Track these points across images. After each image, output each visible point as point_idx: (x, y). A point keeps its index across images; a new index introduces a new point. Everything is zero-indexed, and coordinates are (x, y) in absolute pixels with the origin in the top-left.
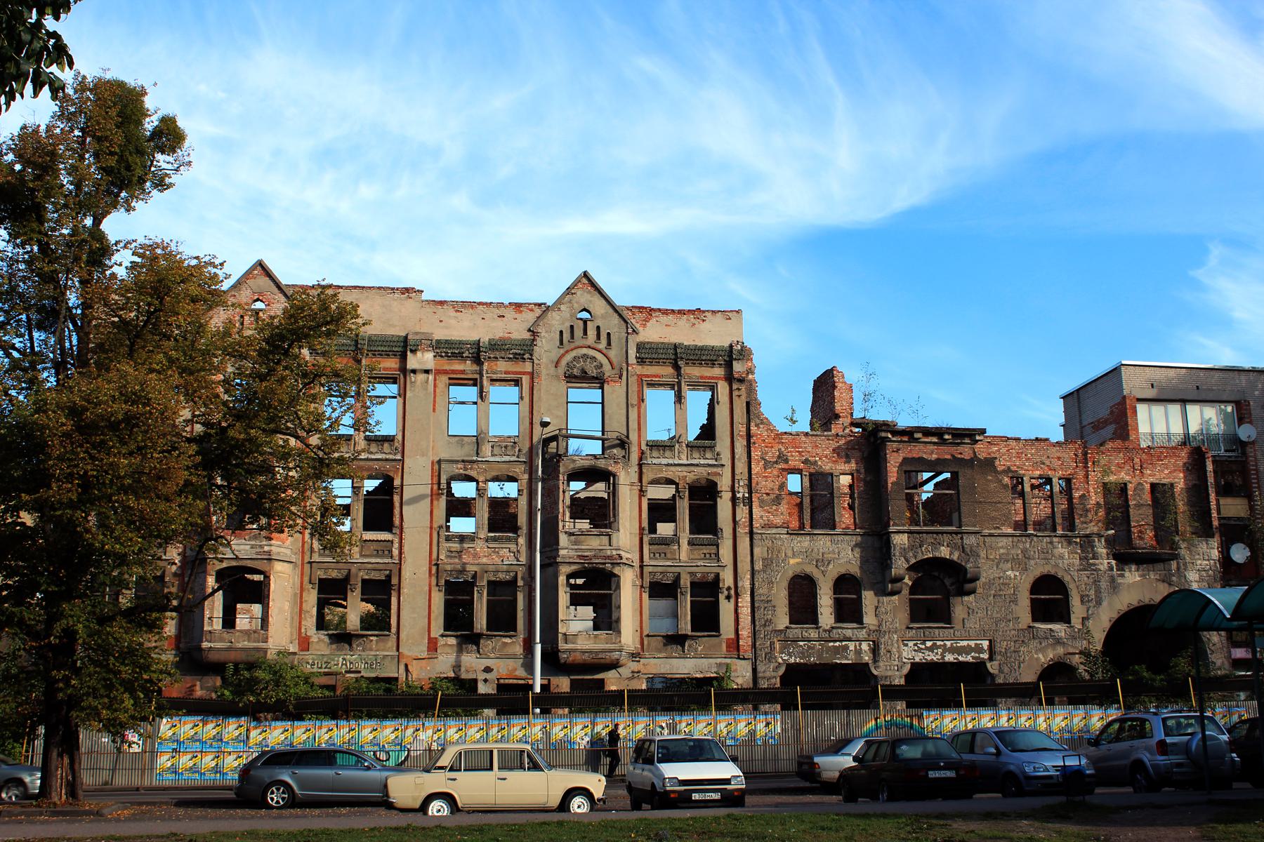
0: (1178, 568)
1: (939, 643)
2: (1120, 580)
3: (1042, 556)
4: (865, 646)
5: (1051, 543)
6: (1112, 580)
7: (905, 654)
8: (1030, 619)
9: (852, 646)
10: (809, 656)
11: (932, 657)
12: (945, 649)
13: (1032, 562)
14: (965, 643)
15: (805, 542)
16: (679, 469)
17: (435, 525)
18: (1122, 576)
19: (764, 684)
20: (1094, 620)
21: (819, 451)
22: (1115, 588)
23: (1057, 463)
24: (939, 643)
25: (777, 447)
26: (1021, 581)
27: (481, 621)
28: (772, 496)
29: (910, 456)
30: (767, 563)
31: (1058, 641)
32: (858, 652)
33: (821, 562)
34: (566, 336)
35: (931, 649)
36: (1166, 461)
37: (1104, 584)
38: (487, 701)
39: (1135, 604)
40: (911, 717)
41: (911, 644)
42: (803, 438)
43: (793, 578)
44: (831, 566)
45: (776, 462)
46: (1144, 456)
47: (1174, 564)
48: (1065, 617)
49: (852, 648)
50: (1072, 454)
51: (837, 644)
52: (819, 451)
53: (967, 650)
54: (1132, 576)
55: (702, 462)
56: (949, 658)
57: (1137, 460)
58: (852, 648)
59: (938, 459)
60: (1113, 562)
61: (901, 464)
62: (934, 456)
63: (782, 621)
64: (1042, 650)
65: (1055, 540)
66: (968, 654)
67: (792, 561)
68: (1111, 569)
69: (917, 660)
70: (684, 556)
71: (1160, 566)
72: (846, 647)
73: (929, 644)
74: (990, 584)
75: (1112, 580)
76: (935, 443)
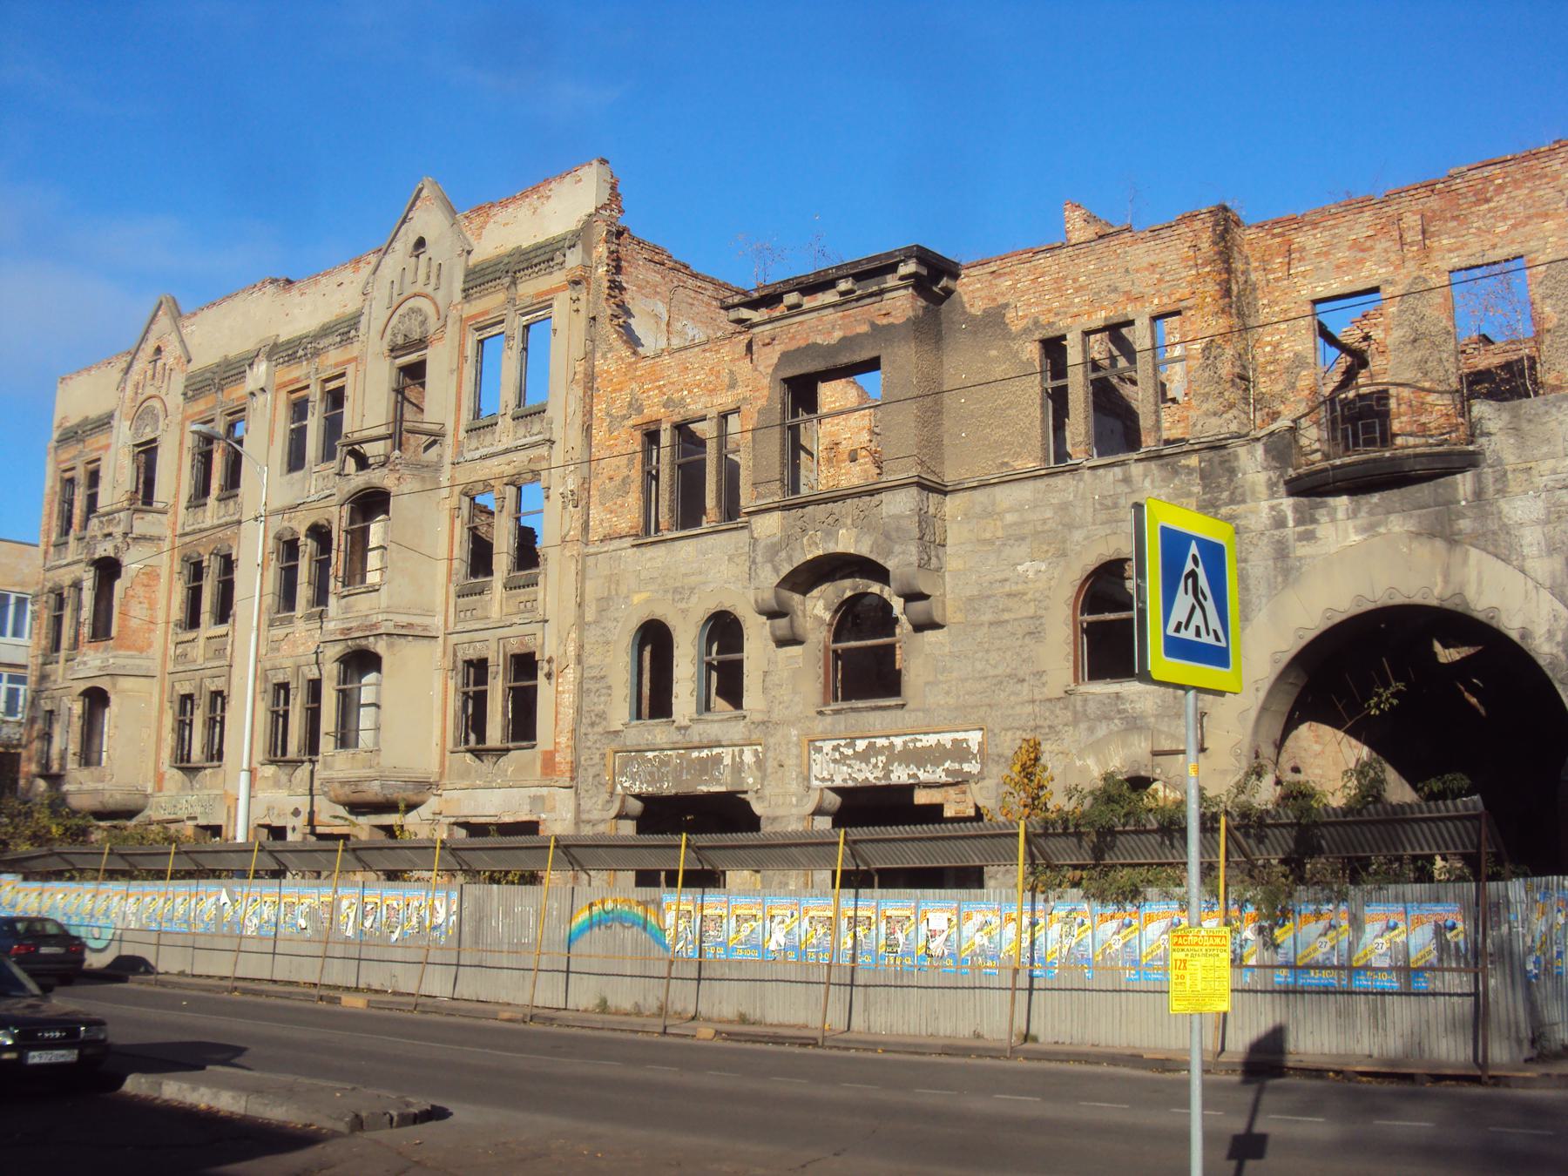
0: (1479, 494)
1: (881, 742)
2: (1302, 549)
3: (1103, 516)
4: (748, 757)
5: (1127, 480)
6: (1281, 552)
7: (816, 769)
8: (1068, 675)
9: (727, 756)
10: (661, 780)
13: (1078, 535)
14: (931, 740)
15: (656, 557)
16: (495, 461)
17: (590, 596)
18: (1309, 537)
22: (1286, 572)
24: (881, 742)
26: (1052, 591)
27: (495, 731)
28: (618, 480)
29: (793, 346)
30: (604, 603)
31: (1134, 724)
32: (738, 767)
35: (864, 757)
36: (1502, 199)
40: (645, 904)
41: (827, 746)
42: (666, 359)
43: (1453, 622)
44: (694, 599)
45: (624, 417)
47: (1464, 483)
49: (727, 760)
50: (1185, 249)
51: (704, 753)
55: (529, 440)
58: (727, 760)
59: (844, 339)
61: (777, 367)
62: (838, 335)
64: (1096, 747)
66: (937, 762)
67: (636, 599)
68: (1280, 523)
70: (495, 612)
71: (1424, 491)
72: (718, 760)
73: (861, 745)
74: (971, 604)
75: (1281, 552)
76: (834, 305)
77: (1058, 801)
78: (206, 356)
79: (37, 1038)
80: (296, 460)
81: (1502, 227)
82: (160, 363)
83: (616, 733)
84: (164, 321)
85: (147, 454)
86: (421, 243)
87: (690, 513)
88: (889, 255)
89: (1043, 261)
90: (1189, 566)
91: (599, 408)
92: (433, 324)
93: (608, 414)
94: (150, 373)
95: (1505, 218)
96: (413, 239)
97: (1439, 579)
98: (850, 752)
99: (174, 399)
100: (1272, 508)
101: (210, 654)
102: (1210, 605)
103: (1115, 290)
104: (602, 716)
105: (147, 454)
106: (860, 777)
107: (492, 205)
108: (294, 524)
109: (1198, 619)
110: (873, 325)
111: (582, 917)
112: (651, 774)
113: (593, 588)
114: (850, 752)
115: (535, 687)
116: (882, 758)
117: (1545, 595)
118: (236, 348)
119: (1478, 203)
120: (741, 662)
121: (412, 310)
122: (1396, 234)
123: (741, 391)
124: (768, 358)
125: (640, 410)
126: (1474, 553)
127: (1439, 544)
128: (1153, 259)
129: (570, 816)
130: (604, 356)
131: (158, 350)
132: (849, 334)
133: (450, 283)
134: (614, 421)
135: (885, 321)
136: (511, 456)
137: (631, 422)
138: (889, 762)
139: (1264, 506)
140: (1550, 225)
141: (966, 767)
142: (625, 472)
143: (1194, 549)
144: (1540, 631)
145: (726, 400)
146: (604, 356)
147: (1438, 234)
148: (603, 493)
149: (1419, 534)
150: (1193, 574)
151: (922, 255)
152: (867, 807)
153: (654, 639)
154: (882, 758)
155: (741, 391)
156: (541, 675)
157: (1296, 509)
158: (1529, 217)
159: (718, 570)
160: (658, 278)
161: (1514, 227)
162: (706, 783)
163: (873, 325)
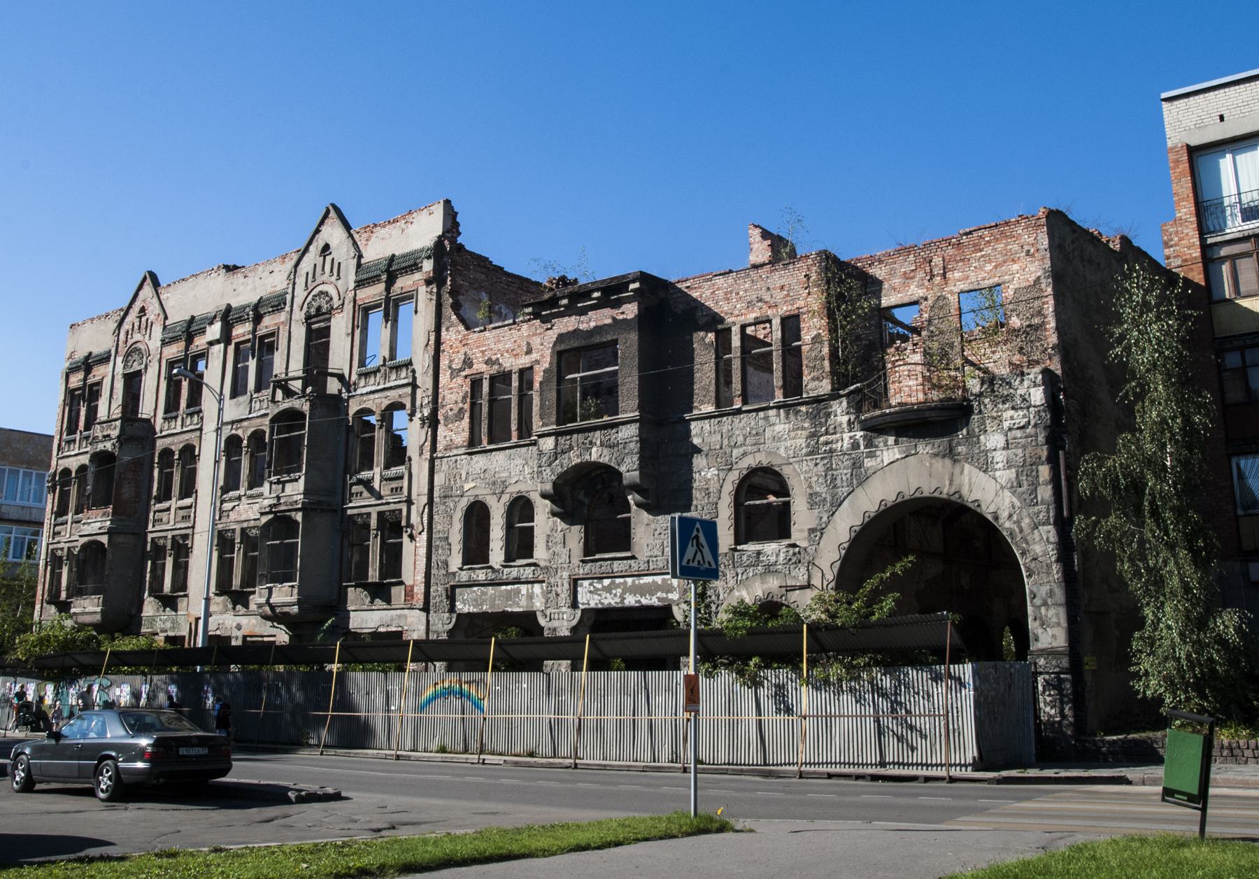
2: (868, 463)
6: (856, 465)
10: (482, 604)
11: (610, 600)
12: (626, 590)
15: (480, 462)
18: (871, 455)
19: (433, 637)
20: (824, 533)
21: (500, 346)
23: (779, 295)
25: (463, 350)
29: (564, 331)
33: (499, 487)
34: (310, 276)
35: (608, 590)
36: (988, 250)
37: (844, 473)
38: (565, 648)
39: (891, 498)
46: (950, 251)
48: (782, 530)
52: (500, 346)
53: (650, 590)
54: (889, 451)
56: (630, 601)
57: (937, 260)
59: (596, 327)
60: (859, 434)
63: (456, 561)
65: (772, 413)
68: (855, 446)
69: (592, 605)
72: (519, 591)
75: (856, 465)
77: (721, 618)
78: (178, 316)
79: (210, 748)
80: (238, 389)
81: (989, 267)
82: (144, 319)
83: (454, 574)
84: (148, 290)
85: (133, 382)
86: (326, 248)
87: (498, 434)
88: (624, 277)
89: (720, 281)
90: (695, 533)
91: (444, 363)
92: (336, 303)
93: (450, 367)
94: (137, 324)
95: (990, 261)
96: (321, 244)
97: (947, 483)
98: (599, 586)
99: (154, 343)
100: (851, 438)
101: (179, 519)
102: (706, 550)
103: (760, 300)
104: (446, 563)
105: (133, 382)
106: (606, 602)
107: (375, 225)
108: (240, 432)
109: (699, 557)
110: (614, 319)
111: (429, 692)
112: (476, 600)
113: (439, 479)
114: (599, 586)
115: (401, 543)
116: (619, 591)
117: (1007, 493)
118: (199, 311)
119: (976, 251)
120: (532, 528)
121: (321, 293)
122: (928, 269)
123: (534, 356)
124: (552, 335)
125: (470, 365)
126: (967, 466)
127: (948, 462)
128: (783, 281)
129: (423, 627)
130: (447, 329)
131: (143, 310)
132: (600, 323)
133: (347, 276)
134: (454, 373)
135: (621, 317)
136: (388, 393)
137: (464, 373)
138: (624, 593)
139: (846, 436)
140: (1016, 267)
141: (670, 596)
142: (461, 405)
143: (698, 525)
144: (1004, 515)
145: (524, 361)
146: (447, 329)
147: (953, 269)
148: (446, 418)
149: (936, 455)
150: (697, 537)
151: (644, 277)
152: (602, 622)
153: (477, 516)
154: (619, 591)
155: (534, 356)
156: (405, 536)
157: (865, 437)
158: (1005, 262)
159: (520, 470)
160: (483, 277)
161: (996, 267)
162: (511, 606)
163: (614, 319)
